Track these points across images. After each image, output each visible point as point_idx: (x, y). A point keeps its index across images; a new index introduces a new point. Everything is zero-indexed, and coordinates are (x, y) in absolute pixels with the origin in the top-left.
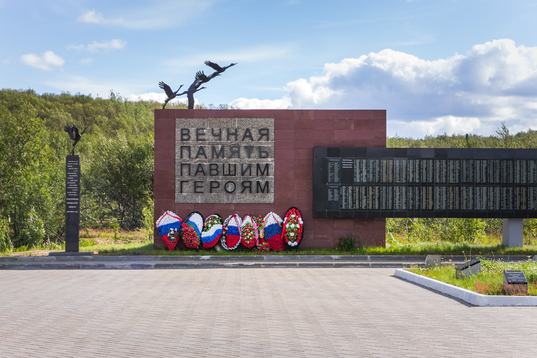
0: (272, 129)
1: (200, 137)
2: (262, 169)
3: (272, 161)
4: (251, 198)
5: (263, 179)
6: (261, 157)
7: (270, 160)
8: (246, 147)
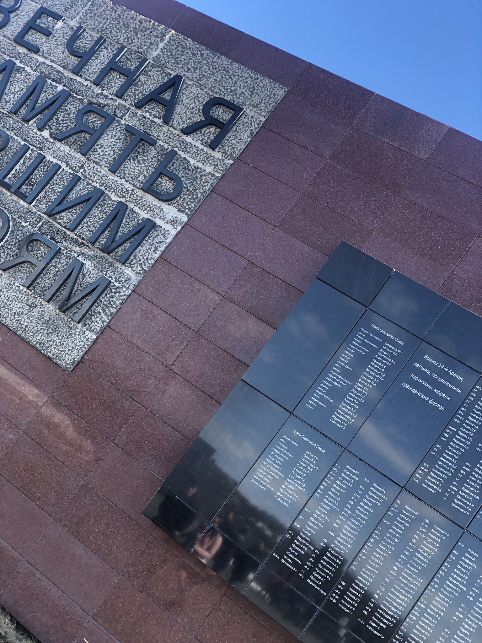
0: (254, 118)
1: (34, 37)
2: (124, 230)
3: (174, 222)
4: (17, 306)
5: (101, 266)
6: (149, 188)
7: (170, 218)
8: (129, 130)
